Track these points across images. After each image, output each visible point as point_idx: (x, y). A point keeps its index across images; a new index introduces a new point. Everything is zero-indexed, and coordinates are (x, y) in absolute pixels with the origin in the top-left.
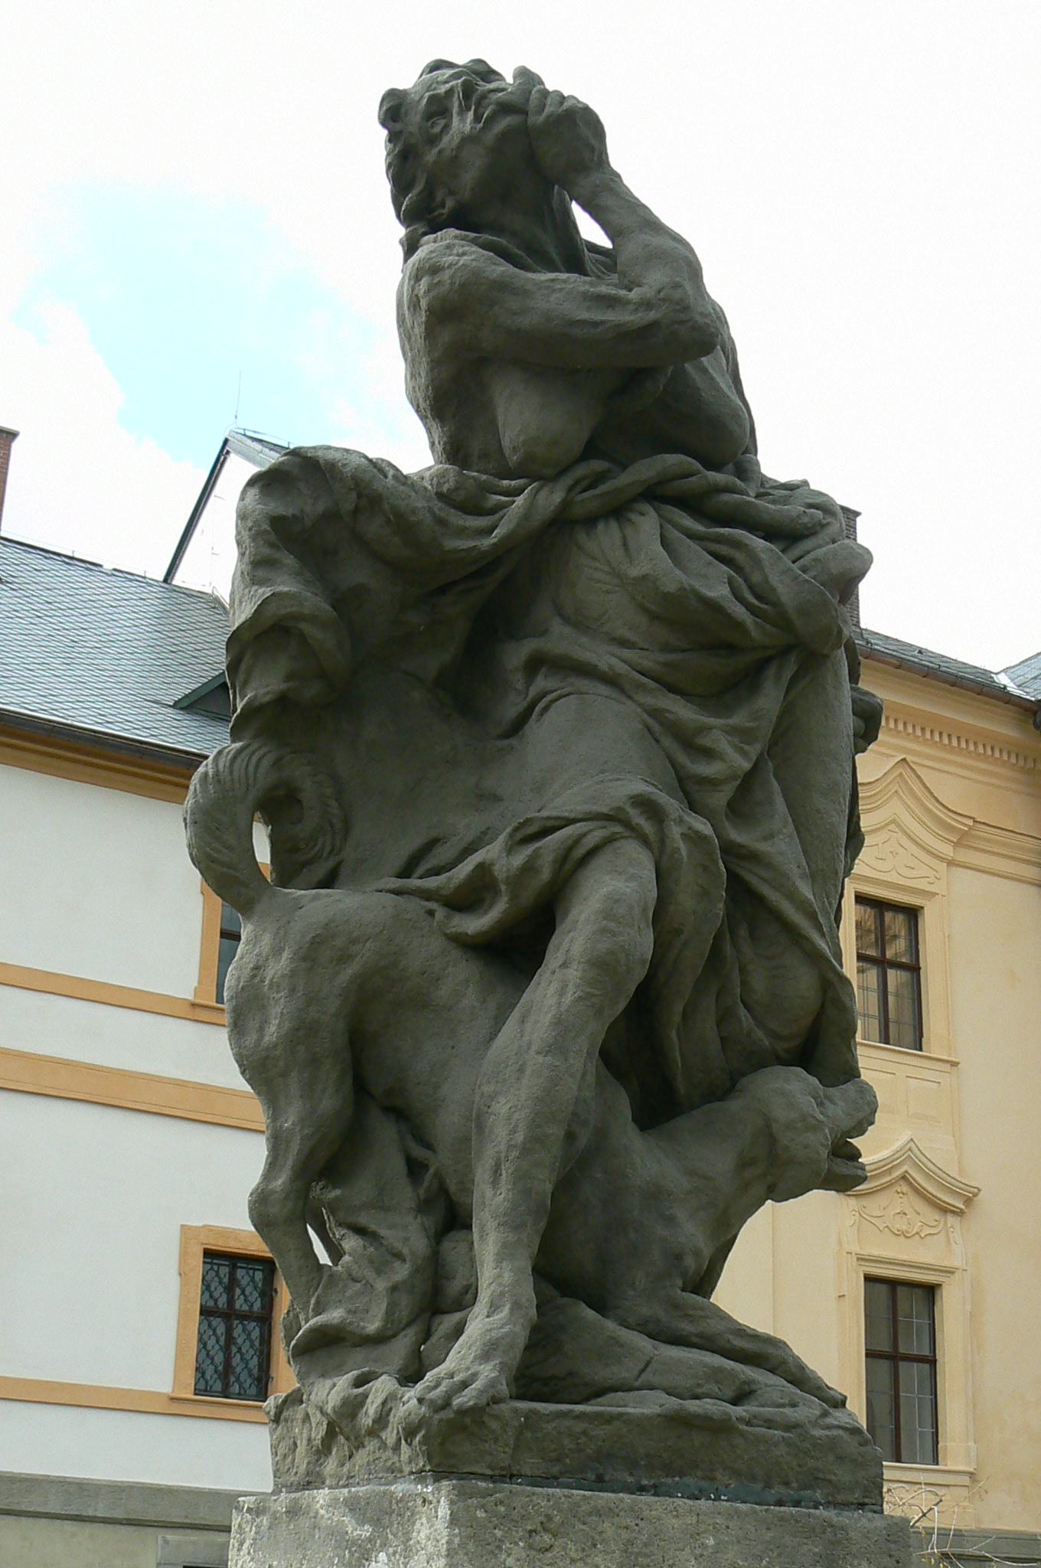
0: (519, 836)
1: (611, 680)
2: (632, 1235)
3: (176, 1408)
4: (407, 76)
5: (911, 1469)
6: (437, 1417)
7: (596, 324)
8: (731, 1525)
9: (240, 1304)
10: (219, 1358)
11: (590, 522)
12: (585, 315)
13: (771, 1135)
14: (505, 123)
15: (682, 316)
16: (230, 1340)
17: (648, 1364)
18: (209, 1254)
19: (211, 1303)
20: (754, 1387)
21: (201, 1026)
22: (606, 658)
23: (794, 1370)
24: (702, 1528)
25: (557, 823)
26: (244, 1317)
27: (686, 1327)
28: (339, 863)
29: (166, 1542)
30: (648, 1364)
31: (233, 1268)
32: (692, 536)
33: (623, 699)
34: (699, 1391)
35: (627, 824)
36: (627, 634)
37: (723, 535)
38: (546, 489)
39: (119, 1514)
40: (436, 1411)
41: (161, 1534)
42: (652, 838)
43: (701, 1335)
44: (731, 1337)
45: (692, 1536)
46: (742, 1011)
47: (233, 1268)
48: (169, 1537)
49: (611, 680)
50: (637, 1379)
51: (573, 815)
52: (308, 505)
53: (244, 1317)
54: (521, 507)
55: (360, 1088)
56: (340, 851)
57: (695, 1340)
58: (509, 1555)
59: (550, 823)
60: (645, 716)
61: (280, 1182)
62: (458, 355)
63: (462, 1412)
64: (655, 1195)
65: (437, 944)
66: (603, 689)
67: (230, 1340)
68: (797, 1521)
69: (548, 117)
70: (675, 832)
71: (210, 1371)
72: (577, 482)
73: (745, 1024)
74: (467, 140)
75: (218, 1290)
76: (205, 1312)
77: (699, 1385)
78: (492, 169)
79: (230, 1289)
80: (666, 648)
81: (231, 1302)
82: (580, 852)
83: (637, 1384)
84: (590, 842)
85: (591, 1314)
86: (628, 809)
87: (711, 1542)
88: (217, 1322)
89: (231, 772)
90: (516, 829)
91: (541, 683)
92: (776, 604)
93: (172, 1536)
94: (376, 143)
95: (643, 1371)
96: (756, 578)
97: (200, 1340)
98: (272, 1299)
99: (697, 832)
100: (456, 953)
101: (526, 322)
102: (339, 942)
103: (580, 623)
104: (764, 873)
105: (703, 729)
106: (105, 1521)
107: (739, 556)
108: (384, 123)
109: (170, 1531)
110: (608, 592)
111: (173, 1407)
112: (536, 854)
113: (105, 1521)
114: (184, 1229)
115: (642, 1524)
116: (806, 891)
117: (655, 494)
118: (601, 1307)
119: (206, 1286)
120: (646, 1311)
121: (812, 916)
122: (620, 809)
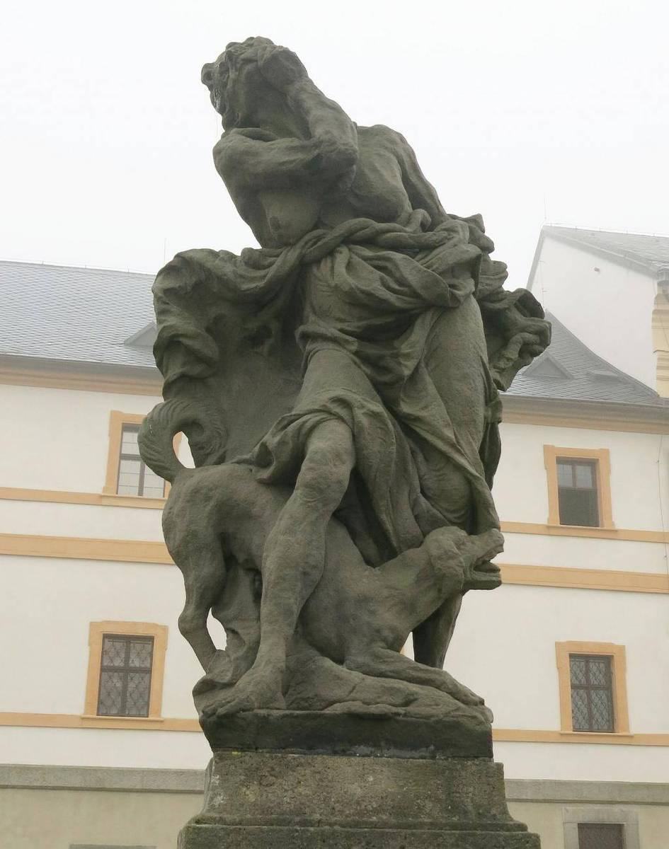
0: (280, 427)
1: (334, 340)
2: (352, 622)
3: (564, 739)
4: (213, 53)
5: (137, 720)
6: (209, 720)
7: (291, 162)
8: (384, 769)
9: (593, 681)
10: (585, 711)
11: (318, 261)
12: (287, 159)
13: (431, 564)
14: (249, 67)
15: (332, 148)
16: (590, 701)
17: (354, 688)
18: (573, 656)
19: (577, 682)
20: (416, 696)
21: (553, 537)
22: (331, 329)
23: (450, 686)
24: (366, 771)
25: (296, 417)
26: (597, 688)
27: (383, 667)
28: (225, 452)
29: (567, 811)
30: (354, 688)
31: (587, 662)
32: (366, 259)
33: (341, 349)
34: (378, 700)
35: (330, 413)
36: (342, 317)
37: (378, 256)
38: (292, 250)
39: (541, 798)
40: (209, 717)
41: (563, 806)
42: (347, 418)
43: (393, 672)
44: (411, 671)
45: (360, 777)
46: (422, 499)
47: (587, 662)
48: (568, 808)
49: (334, 340)
50: (348, 696)
51: (301, 413)
52: (189, 281)
53: (597, 688)
54: (289, 257)
55: (229, 560)
56: (224, 446)
57: (390, 674)
58: (248, 789)
59: (293, 418)
60: (352, 356)
61: (189, 612)
62: (249, 187)
63: (220, 717)
64: (364, 600)
65: (253, 486)
66: (331, 345)
67: (590, 701)
68: (427, 767)
69: (265, 60)
70: (359, 413)
71: (581, 718)
72: (306, 243)
73: (424, 505)
74: (235, 81)
75: (580, 676)
76: (574, 687)
77: (379, 697)
78: (258, 89)
79: (587, 673)
80: (360, 319)
81: (588, 680)
82: (304, 431)
83: (348, 698)
84: (309, 425)
85: (328, 663)
86: (328, 405)
87: (371, 779)
88: (581, 692)
89: (159, 416)
90: (278, 423)
91: (309, 347)
92: (409, 286)
93: (570, 808)
94: (205, 92)
95: (351, 692)
96: (398, 275)
97: (573, 702)
98: (610, 677)
99: (372, 412)
100: (262, 489)
101: (260, 169)
102: (204, 491)
103: (323, 314)
104: (419, 425)
105: (381, 357)
106: (532, 801)
107: (388, 265)
108: (204, 82)
109: (568, 805)
110: (329, 296)
111: (561, 739)
112: (286, 435)
113: (532, 801)
114: (558, 645)
115: (329, 771)
116: (449, 433)
117: (349, 240)
118: (340, 661)
119: (574, 674)
120: (360, 659)
121: (453, 446)
122: (324, 406)
